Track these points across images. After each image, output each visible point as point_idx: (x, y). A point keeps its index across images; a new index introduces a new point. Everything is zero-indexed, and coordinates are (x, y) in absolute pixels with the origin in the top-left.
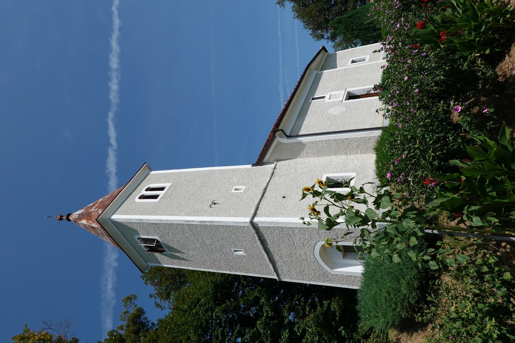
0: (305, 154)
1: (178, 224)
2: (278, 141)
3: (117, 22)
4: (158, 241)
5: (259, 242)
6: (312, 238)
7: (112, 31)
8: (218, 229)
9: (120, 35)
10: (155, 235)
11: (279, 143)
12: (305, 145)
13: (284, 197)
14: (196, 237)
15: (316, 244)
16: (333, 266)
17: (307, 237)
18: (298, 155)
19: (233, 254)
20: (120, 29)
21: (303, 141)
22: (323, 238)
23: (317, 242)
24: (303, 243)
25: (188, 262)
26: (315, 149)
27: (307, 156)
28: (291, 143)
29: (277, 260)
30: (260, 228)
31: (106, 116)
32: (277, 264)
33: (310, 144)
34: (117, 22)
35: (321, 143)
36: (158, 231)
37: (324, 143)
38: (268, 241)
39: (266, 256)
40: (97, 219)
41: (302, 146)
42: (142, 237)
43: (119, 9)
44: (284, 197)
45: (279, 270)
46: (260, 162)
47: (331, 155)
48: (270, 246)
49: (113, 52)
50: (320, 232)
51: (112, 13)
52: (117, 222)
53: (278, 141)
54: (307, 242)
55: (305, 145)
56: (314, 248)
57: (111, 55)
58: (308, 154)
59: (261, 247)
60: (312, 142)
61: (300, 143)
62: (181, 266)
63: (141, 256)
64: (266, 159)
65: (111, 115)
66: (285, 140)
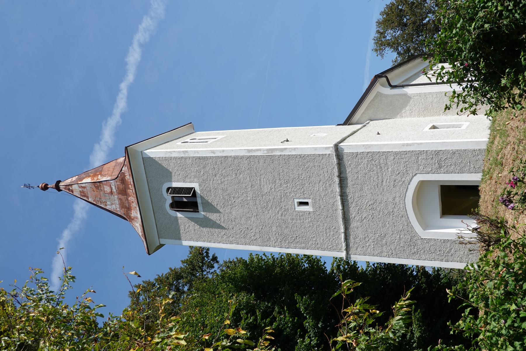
0: (408, 113)
1: (236, 158)
2: (378, 92)
3: (121, 104)
4: (194, 194)
5: (337, 180)
6: (408, 169)
7: (110, 114)
8: (288, 163)
9: (121, 122)
10: (195, 180)
11: (379, 94)
12: (411, 98)
13: (378, 134)
14: (252, 180)
15: (412, 179)
16: (426, 226)
17: (402, 169)
18: (398, 113)
19: (295, 208)
20: (123, 116)
21: (409, 93)
22: (423, 168)
23: (413, 177)
24: (395, 181)
25: (223, 232)
26: (423, 104)
27: (410, 115)
28: (394, 95)
29: (353, 216)
30: (345, 157)
31: (59, 235)
32: (352, 226)
33: (417, 97)
34: (121, 104)
35: (431, 96)
36: (202, 171)
37: (435, 96)
38: (349, 181)
39: (340, 207)
40: (128, 148)
41: (407, 98)
42: (175, 185)
43: (131, 89)
44: (378, 134)
45: (351, 237)
46: (347, 122)
47: (440, 114)
48: (350, 190)
49: (102, 143)
50: (420, 158)
51: (119, 90)
52: (150, 158)
53: (378, 92)
54: (400, 179)
55: (411, 98)
56: (407, 188)
57: (97, 147)
58: (412, 112)
59: (338, 190)
60: (420, 95)
61: (405, 95)
62: (210, 242)
63: (156, 226)
64: (357, 117)
65: (67, 235)
66: (387, 91)
